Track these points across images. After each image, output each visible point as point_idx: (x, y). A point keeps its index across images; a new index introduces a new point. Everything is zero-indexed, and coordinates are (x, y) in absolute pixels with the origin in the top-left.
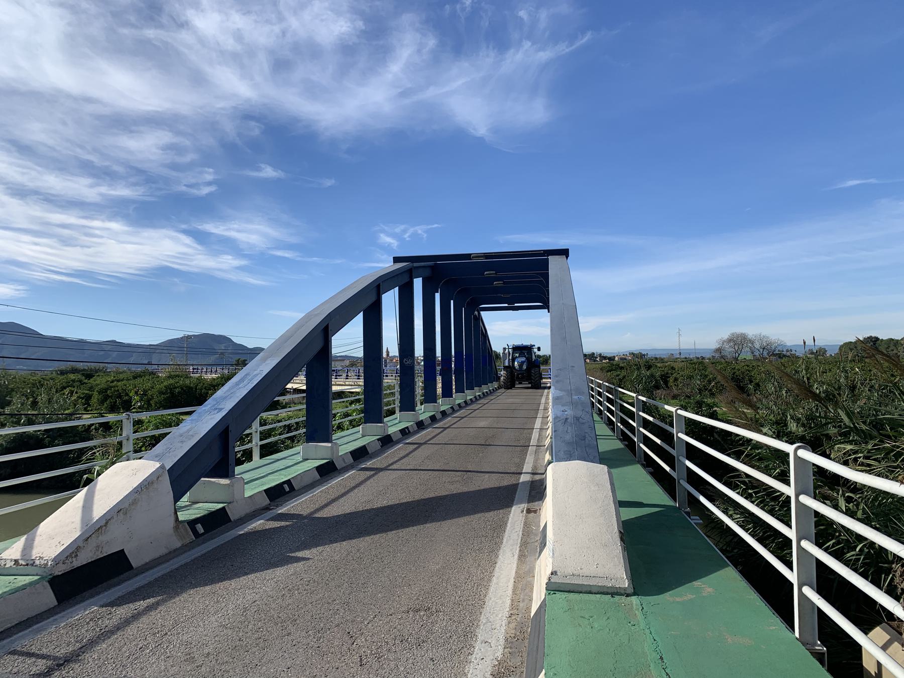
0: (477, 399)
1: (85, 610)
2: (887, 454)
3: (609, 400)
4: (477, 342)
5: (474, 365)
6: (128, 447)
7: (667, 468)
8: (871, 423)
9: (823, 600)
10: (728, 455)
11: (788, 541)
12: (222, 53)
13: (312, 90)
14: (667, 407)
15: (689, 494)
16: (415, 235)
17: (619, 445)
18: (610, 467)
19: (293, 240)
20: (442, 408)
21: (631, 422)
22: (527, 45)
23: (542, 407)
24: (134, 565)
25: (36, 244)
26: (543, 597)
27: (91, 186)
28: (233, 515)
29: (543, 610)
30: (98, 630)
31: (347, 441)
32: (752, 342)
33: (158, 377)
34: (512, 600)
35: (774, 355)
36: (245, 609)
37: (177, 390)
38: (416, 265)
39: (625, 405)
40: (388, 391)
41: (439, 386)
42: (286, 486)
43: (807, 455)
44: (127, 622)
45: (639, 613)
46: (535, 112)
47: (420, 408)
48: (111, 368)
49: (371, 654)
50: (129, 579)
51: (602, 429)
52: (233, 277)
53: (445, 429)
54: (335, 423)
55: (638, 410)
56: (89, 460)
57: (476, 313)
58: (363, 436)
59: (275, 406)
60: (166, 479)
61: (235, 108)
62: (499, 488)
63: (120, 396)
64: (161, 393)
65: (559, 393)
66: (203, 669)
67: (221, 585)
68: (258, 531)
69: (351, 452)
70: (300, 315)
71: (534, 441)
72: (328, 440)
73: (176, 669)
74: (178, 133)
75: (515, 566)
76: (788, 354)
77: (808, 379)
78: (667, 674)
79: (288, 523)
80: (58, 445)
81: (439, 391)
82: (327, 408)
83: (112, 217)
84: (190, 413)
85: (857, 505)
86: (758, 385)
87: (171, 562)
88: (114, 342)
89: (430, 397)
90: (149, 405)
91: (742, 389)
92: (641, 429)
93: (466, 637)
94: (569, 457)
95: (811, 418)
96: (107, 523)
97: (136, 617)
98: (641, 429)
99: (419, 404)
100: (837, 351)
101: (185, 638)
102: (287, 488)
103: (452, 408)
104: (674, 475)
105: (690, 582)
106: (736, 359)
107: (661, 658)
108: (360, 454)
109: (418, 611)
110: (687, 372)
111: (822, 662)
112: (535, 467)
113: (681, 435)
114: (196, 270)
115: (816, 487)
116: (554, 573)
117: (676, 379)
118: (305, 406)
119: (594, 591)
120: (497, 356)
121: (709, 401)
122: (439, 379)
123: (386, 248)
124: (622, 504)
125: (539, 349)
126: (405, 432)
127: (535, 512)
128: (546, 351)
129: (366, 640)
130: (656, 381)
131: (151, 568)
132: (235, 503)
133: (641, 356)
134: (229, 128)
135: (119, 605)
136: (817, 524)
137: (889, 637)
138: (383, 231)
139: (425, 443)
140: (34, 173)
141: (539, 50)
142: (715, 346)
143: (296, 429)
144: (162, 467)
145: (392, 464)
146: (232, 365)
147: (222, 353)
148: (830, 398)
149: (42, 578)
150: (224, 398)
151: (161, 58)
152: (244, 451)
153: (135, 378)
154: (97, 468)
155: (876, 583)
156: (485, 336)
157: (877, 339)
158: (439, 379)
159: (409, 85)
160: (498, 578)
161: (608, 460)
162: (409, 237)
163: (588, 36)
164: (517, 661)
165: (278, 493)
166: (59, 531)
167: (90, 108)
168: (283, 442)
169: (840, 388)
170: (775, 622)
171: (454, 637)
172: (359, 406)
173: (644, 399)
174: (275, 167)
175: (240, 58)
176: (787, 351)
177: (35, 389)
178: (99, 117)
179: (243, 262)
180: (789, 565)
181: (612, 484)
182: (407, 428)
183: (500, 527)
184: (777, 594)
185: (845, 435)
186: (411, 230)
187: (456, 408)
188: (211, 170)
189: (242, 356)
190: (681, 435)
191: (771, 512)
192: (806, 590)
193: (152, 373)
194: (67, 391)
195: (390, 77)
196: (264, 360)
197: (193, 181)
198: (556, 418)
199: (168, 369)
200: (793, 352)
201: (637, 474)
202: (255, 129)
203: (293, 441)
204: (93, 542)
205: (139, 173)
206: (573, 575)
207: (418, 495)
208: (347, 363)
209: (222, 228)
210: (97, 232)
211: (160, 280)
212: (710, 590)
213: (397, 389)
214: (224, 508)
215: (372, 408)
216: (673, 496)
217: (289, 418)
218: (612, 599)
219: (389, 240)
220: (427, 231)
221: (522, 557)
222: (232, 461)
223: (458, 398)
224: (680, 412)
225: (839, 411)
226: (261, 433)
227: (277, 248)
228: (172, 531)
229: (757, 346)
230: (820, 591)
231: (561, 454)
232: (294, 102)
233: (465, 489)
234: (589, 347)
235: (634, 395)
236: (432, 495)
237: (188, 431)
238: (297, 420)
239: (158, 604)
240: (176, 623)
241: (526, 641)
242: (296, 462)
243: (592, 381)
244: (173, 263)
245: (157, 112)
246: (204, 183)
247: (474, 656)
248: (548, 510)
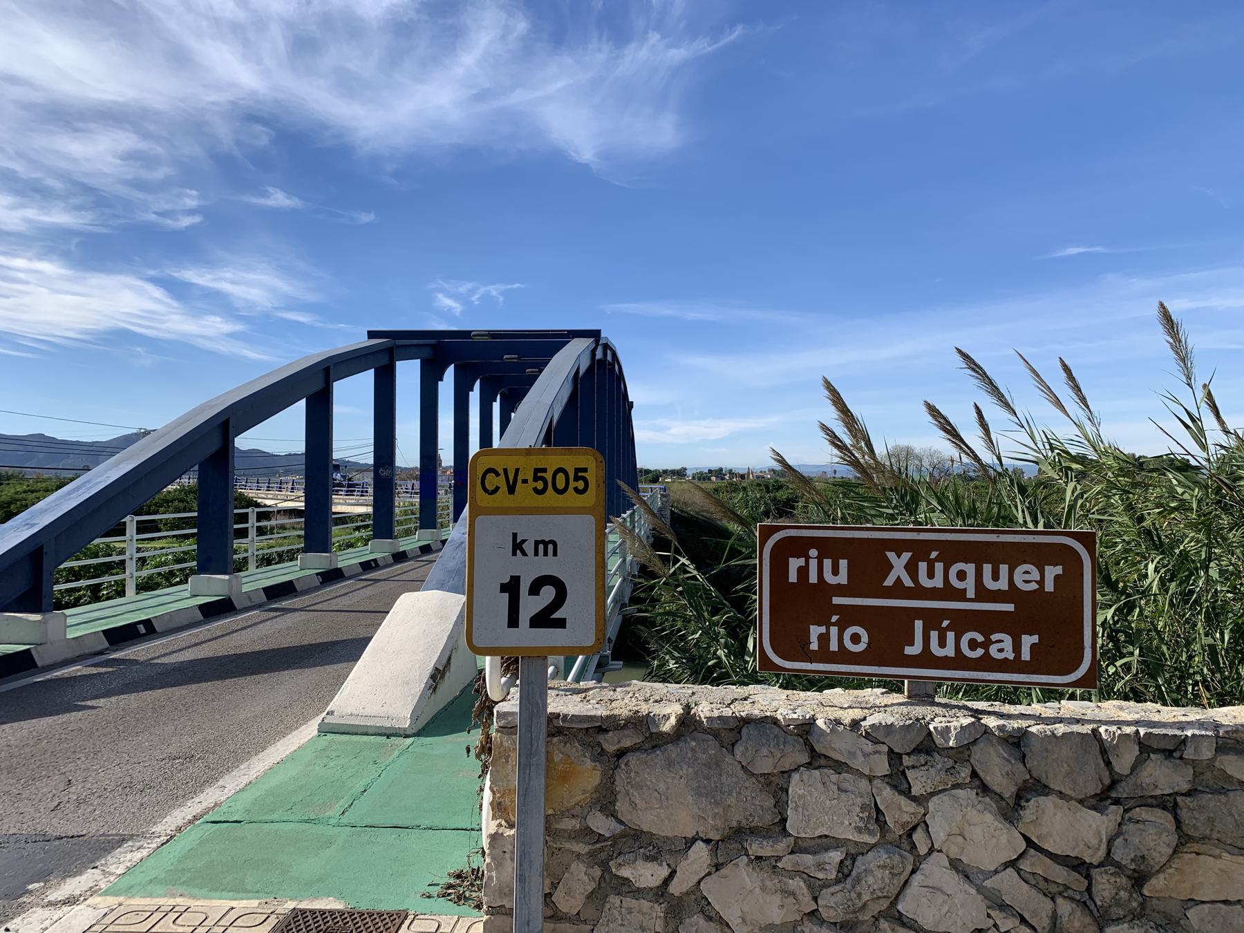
12: (217, 22)
13: (348, 85)
16: (486, 298)
19: (311, 297)
27: (13, 208)
46: (661, 133)
48: (30, 474)
52: (223, 348)
69: (264, 589)
74: (146, 136)
83: (44, 255)
102: (142, 629)
114: (167, 336)
118: (302, 533)
119: (370, 731)
130: (766, 504)
134: (224, 132)
138: (441, 290)
141: (670, 46)
150: (43, 511)
162: (479, 299)
163: (738, 31)
167: (15, 92)
178: (28, 106)
186: (482, 290)
188: (194, 193)
195: (460, 71)
197: (168, 207)
202: (262, 137)
205: (85, 192)
210: (21, 276)
214: (28, 650)
219: (449, 302)
220: (502, 293)
227: (288, 308)
229: (926, 463)
232: (320, 99)
244: (139, 325)
245: (116, 103)
246: (184, 209)
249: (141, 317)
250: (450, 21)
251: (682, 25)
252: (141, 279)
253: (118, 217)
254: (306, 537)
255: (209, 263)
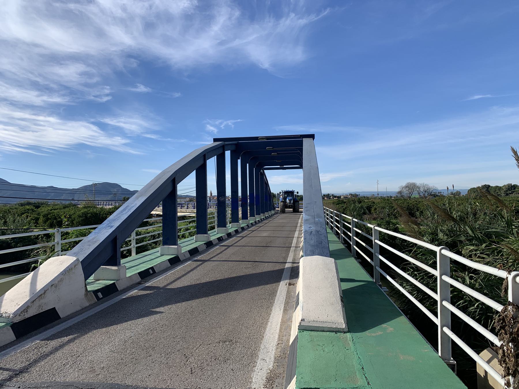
0: (262, 220)
1: (32, 343)
2: (493, 251)
3: (337, 221)
4: (262, 189)
5: (261, 201)
6: (58, 248)
7: (369, 260)
8: (485, 233)
9: (455, 335)
10: (403, 253)
11: (436, 302)
12: (114, 18)
13: (167, 41)
14: (369, 225)
15: (381, 274)
16: (227, 126)
17: (342, 246)
18: (335, 259)
19: (157, 128)
20: (242, 226)
21: (349, 233)
22: (292, 15)
23: (299, 225)
24: (61, 317)
25: (6, 130)
26: (296, 334)
27: (38, 96)
28: (120, 287)
29: (296, 341)
30: (39, 354)
31: (187, 244)
32: (419, 188)
33: (78, 207)
34: (279, 336)
35: (431, 195)
36: (125, 342)
37: (89, 215)
38: (226, 143)
39: (346, 224)
40: (211, 216)
41: (240, 213)
42: (150, 270)
43: (447, 253)
44: (56, 349)
45: (351, 343)
46: (297, 55)
47: (229, 225)
48: (50, 202)
49: (197, 367)
50: (59, 324)
51: (332, 237)
52: (122, 149)
53: (243, 237)
54: (180, 234)
55: (353, 227)
56: (35, 256)
57: (262, 171)
58: (196, 242)
59: (146, 224)
60: (80, 267)
61: (122, 51)
62: (273, 271)
63: (55, 219)
64: (80, 216)
65: (308, 217)
66: (100, 376)
67: (112, 328)
68: (134, 297)
70: (159, 172)
71: (294, 244)
72: (175, 244)
73: (84, 376)
74: (89, 65)
75: (281, 316)
76: (439, 194)
77: (450, 209)
78: (366, 377)
79: (151, 292)
80: (20, 247)
81: (240, 215)
82: (175, 225)
83: (51, 114)
84: (95, 228)
85: (476, 281)
86: (422, 212)
87: (83, 314)
88: (52, 187)
89: (235, 219)
90: (73, 223)
91: (412, 214)
92: (355, 238)
93: (251, 357)
94: (313, 254)
95: (451, 231)
96: (45, 292)
97: (61, 346)
98: (355, 238)
99: (228, 223)
100: (466, 193)
101: (90, 358)
103: (247, 225)
104: (373, 263)
105: (381, 324)
106: (410, 197)
107: (363, 368)
108: (194, 252)
109: (225, 342)
110: (382, 205)
111: (453, 370)
112: (294, 259)
113: (377, 241)
114: (99, 145)
115: (452, 271)
116: (303, 320)
117: (375, 209)
118: (162, 225)
119: (325, 330)
120: (274, 196)
121: (394, 221)
122: (240, 209)
123: (210, 133)
124: (342, 280)
125: (298, 193)
126: (220, 239)
127: (294, 285)
128: (301, 193)
129: (195, 359)
130: (364, 210)
131: (72, 318)
132: (121, 281)
133: (356, 195)
134: (119, 63)
135: (52, 340)
136: (452, 292)
137: (491, 356)
138: (209, 123)
139: (231, 246)
140: (4, 88)
141: (299, 18)
142: (397, 190)
143: (158, 238)
144: (77, 260)
145: (212, 258)
146: (121, 201)
147: (115, 194)
148: (462, 220)
149: (7, 324)
150: (114, 220)
151: (77, 20)
152: (128, 250)
153: (64, 208)
154: (40, 260)
155: (485, 326)
156: (267, 184)
157: (489, 186)
158: (240, 209)
159: (224, 38)
160: (271, 323)
161: (335, 255)
162: (224, 127)
164: (281, 370)
165: (146, 275)
166: (18, 296)
167: (37, 50)
168: (150, 245)
169: (468, 214)
170: (428, 347)
171: (246, 357)
172: (194, 224)
173: (356, 220)
174: (146, 86)
175: (125, 21)
176: (439, 193)
177: (6, 214)
178: (42, 56)
179: (128, 141)
180: (436, 315)
181: (337, 269)
182: (221, 237)
183: (273, 294)
184: (428, 331)
185: (470, 240)
186: (225, 123)
187: (250, 225)
188: (108, 87)
189: (126, 195)
190: (377, 241)
191: (427, 285)
192: (446, 329)
193: (75, 205)
194: (24, 216)
195: (212, 33)
196: (137, 198)
197: (98, 93)
198: (305, 231)
199: (84, 203)
200: (442, 194)
201: (352, 263)
202: (134, 64)
203: (156, 244)
204: (37, 303)
205: (65, 89)
206: (314, 321)
207: (227, 276)
208: (188, 199)
209: (115, 121)
210: (42, 123)
211: (78, 151)
212: (392, 329)
213: (216, 215)
214: (114, 283)
215: (201, 225)
216: (372, 276)
217: (154, 231)
218: (336, 335)
219: (212, 128)
220: (234, 124)
221: (285, 310)
222: (119, 255)
223: (251, 220)
224: (376, 228)
225: (467, 227)
226: (136, 240)
227: (147, 133)
228: (84, 297)
229: (422, 190)
230: (453, 330)
231: (308, 252)
232: (157, 48)
233: (254, 272)
234: (326, 190)
235: (351, 218)
236: (234, 275)
237: (93, 239)
238: (159, 232)
239: (75, 339)
240: (85, 350)
241: (287, 359)
242: (157, 257)
243: (327, 210)
246: (104, 93)
247: (256, 368)
248: (300, 283)
249: (89, 138)
250: (208, 13)
251: (304, 9)
252: (88, 123)
253: (79, 98)
254: (197, 227)
255: (114, 115)
